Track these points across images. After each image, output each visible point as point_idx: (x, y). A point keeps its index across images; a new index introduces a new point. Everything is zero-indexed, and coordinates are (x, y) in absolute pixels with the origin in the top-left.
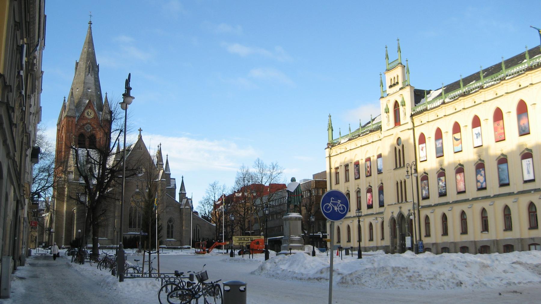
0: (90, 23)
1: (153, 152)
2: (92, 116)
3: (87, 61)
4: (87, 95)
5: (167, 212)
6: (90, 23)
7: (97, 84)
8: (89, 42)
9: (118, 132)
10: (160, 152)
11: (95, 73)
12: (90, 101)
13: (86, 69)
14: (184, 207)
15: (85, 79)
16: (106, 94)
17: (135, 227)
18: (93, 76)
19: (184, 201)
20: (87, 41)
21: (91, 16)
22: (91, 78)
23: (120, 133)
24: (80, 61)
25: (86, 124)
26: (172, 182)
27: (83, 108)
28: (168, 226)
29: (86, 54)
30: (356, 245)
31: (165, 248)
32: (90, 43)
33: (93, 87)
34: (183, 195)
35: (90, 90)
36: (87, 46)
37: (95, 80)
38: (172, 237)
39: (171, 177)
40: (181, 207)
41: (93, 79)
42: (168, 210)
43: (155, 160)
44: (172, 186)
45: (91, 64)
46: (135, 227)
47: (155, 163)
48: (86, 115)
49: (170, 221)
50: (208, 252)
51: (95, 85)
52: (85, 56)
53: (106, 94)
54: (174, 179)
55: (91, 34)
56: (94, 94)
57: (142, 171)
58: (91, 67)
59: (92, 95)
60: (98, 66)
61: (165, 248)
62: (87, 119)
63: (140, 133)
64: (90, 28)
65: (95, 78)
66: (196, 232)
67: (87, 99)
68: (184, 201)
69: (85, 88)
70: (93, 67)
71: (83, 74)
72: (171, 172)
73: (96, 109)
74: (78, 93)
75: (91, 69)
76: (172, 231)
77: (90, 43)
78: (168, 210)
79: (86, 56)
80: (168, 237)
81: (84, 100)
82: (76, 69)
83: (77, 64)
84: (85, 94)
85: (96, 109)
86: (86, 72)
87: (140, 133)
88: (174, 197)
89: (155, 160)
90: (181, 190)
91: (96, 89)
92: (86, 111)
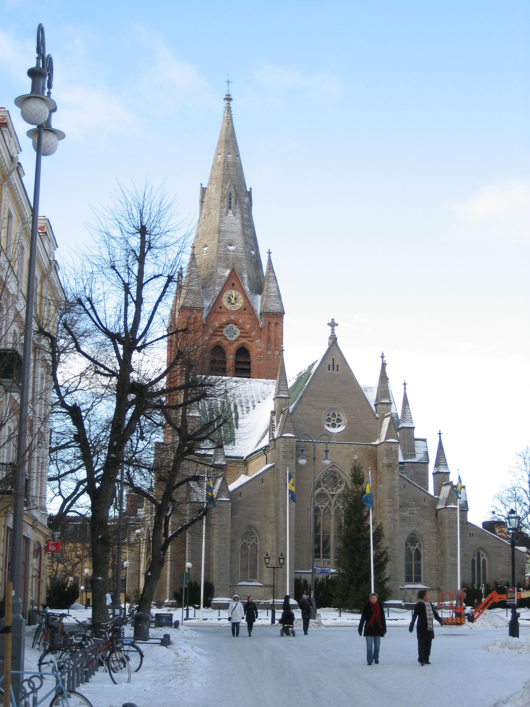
0: (228, 99)
1: (367, 379)
2: (239, 304)
3: (225, 182)
4: (227, 259)
5: (403, 520)
6: (228, 99)
7: (249, 232)
8: (226, 141)
9: (163, 281)
10: (384, 378)
11: (242, 209)
12: (233, 270)
13: (222, 201)
14: (444, 508)
15: (221, 222)
16: (269, 253)
17: (328, 557)
18: (238, 215)
19: (446, 491)
20: (223, 138)
21: (228, 82)
22: (233, 221)
23: (166, 286)
24: (210, 183)
25: (227, 324)
26: (419, 448)
27: (218, 289)
28: (408, 552)
29: (221, 167)
30: (58, 458)
31: (399, 606)
32: (230, 141)
33: (239, 240)
34: (442, 477)
35: (231, 248)
36: (222, 150)
37: (243, 225)
38: (418, 580)
39: (417, 435)
40: (439, 507)
41: (238, 221)
42: (406, 514)
43: (372, 397)
44: (419, 457)
45: (232, 189)
46: (328, 557)
47: (372, 403)
48: (225, 303)
49: (413, 540)
50: (472, 619)
51: (244, 234)
52: (219, 172)
53: (269, 253)
54: (424, 440)
55: (229, 121)
56: (242, 255)
57: (339, 420)
58: (233, 194)
59: (237, 258)
60: (249, 194)
61: (399, 606)
62: (228, 311)
63: (333, 330)
64: (229, 109)
65: (243, 219)
66: (475, 565)
67: (227, 267)
68: (446, 491)
69: (223, 244)
70: (237, 195)
71: (215, 214)
72: (415, 424)
73: (247, 288)
74: (206, 254)
75: (233, 200)
76: (418, 567)
77: (230, 141)
78: (406, 514)
79: (221, 172)
80: (409, 580)
81: (219, 269)
82: (202, 202)
83: (203, 191)
84: (223, 258)
85: (247, 288)
86: (221, 208)
87: (333, 330)
88: (425, 484)
89: (372, 397)
90: (437, 465)
91: (246, 243)
92: (225, 296)
